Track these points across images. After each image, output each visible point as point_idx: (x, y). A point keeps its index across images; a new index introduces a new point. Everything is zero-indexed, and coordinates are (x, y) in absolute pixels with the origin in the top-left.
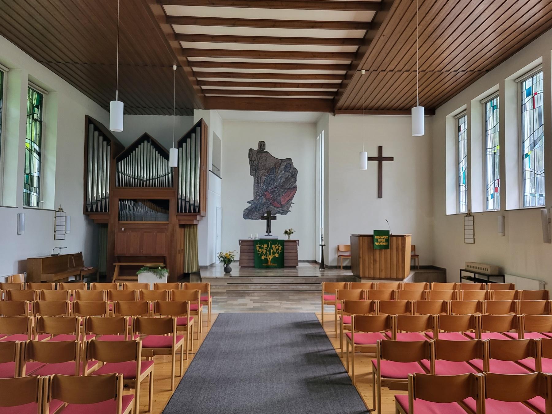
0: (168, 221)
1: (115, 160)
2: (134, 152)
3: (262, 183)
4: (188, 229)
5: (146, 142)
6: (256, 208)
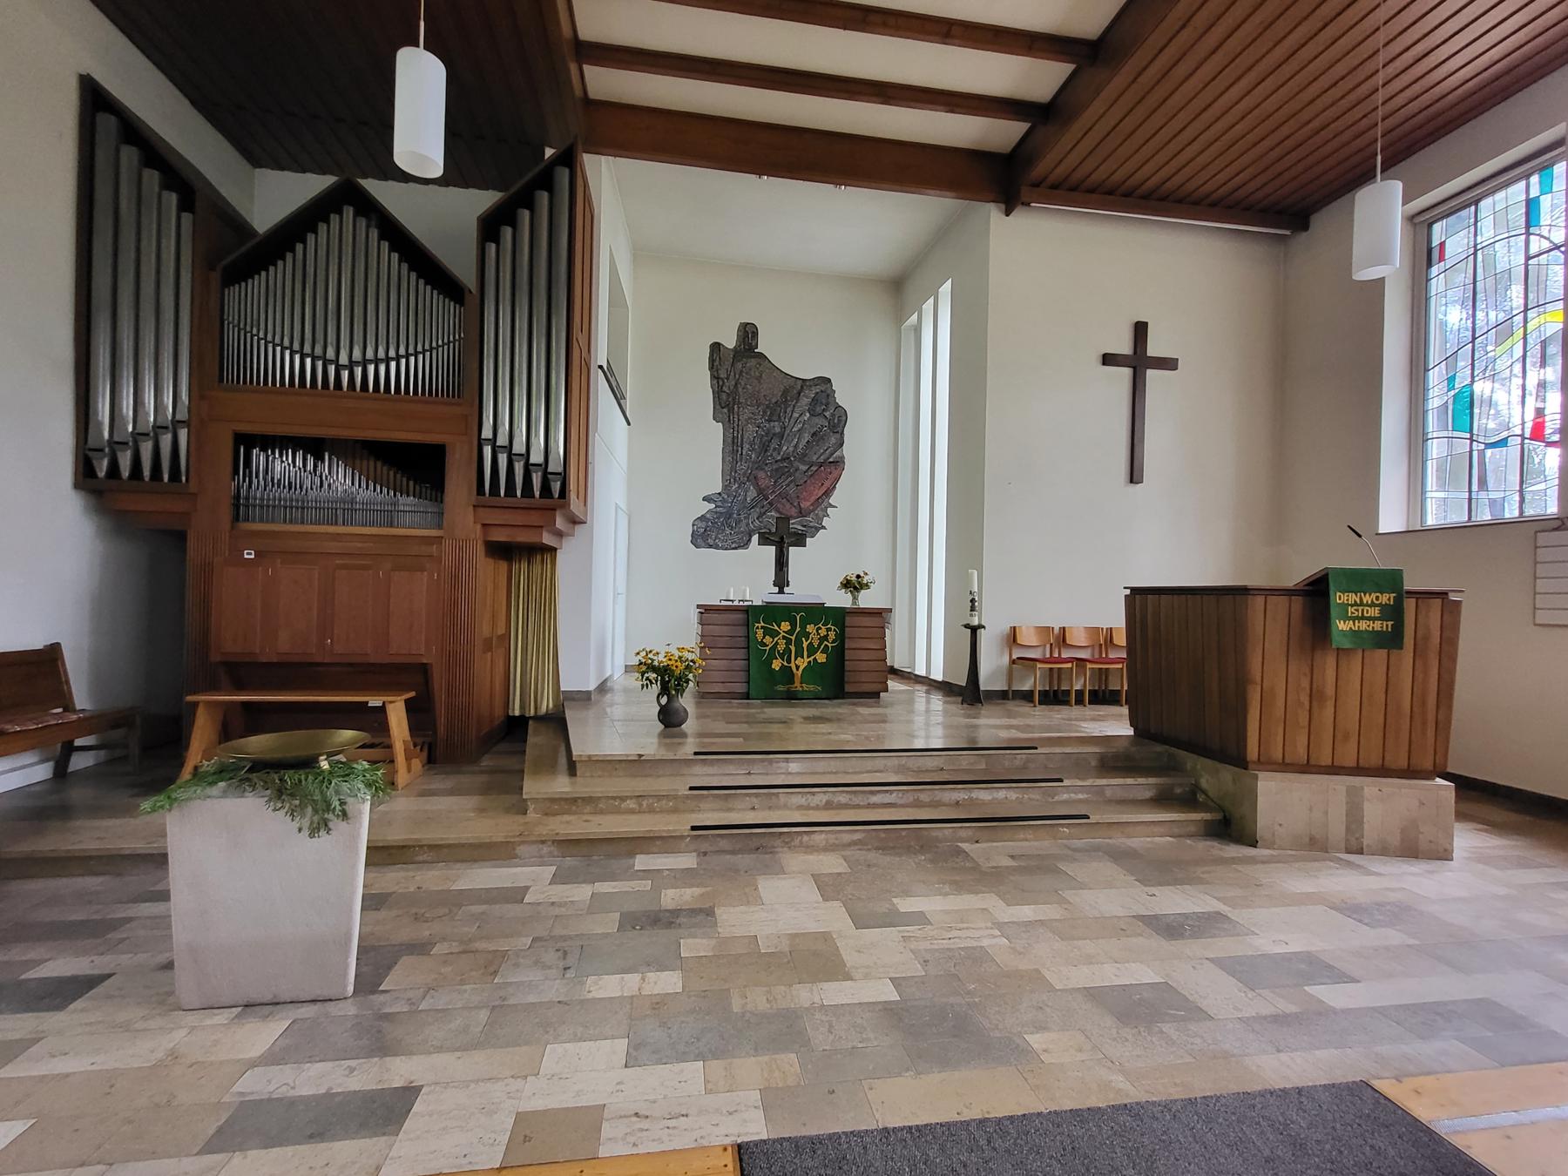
0: (440, 527)
1: (216, 277)
3: (746, 446)
4: (524, 565)
5: (349, 212)
6: (729, 515)
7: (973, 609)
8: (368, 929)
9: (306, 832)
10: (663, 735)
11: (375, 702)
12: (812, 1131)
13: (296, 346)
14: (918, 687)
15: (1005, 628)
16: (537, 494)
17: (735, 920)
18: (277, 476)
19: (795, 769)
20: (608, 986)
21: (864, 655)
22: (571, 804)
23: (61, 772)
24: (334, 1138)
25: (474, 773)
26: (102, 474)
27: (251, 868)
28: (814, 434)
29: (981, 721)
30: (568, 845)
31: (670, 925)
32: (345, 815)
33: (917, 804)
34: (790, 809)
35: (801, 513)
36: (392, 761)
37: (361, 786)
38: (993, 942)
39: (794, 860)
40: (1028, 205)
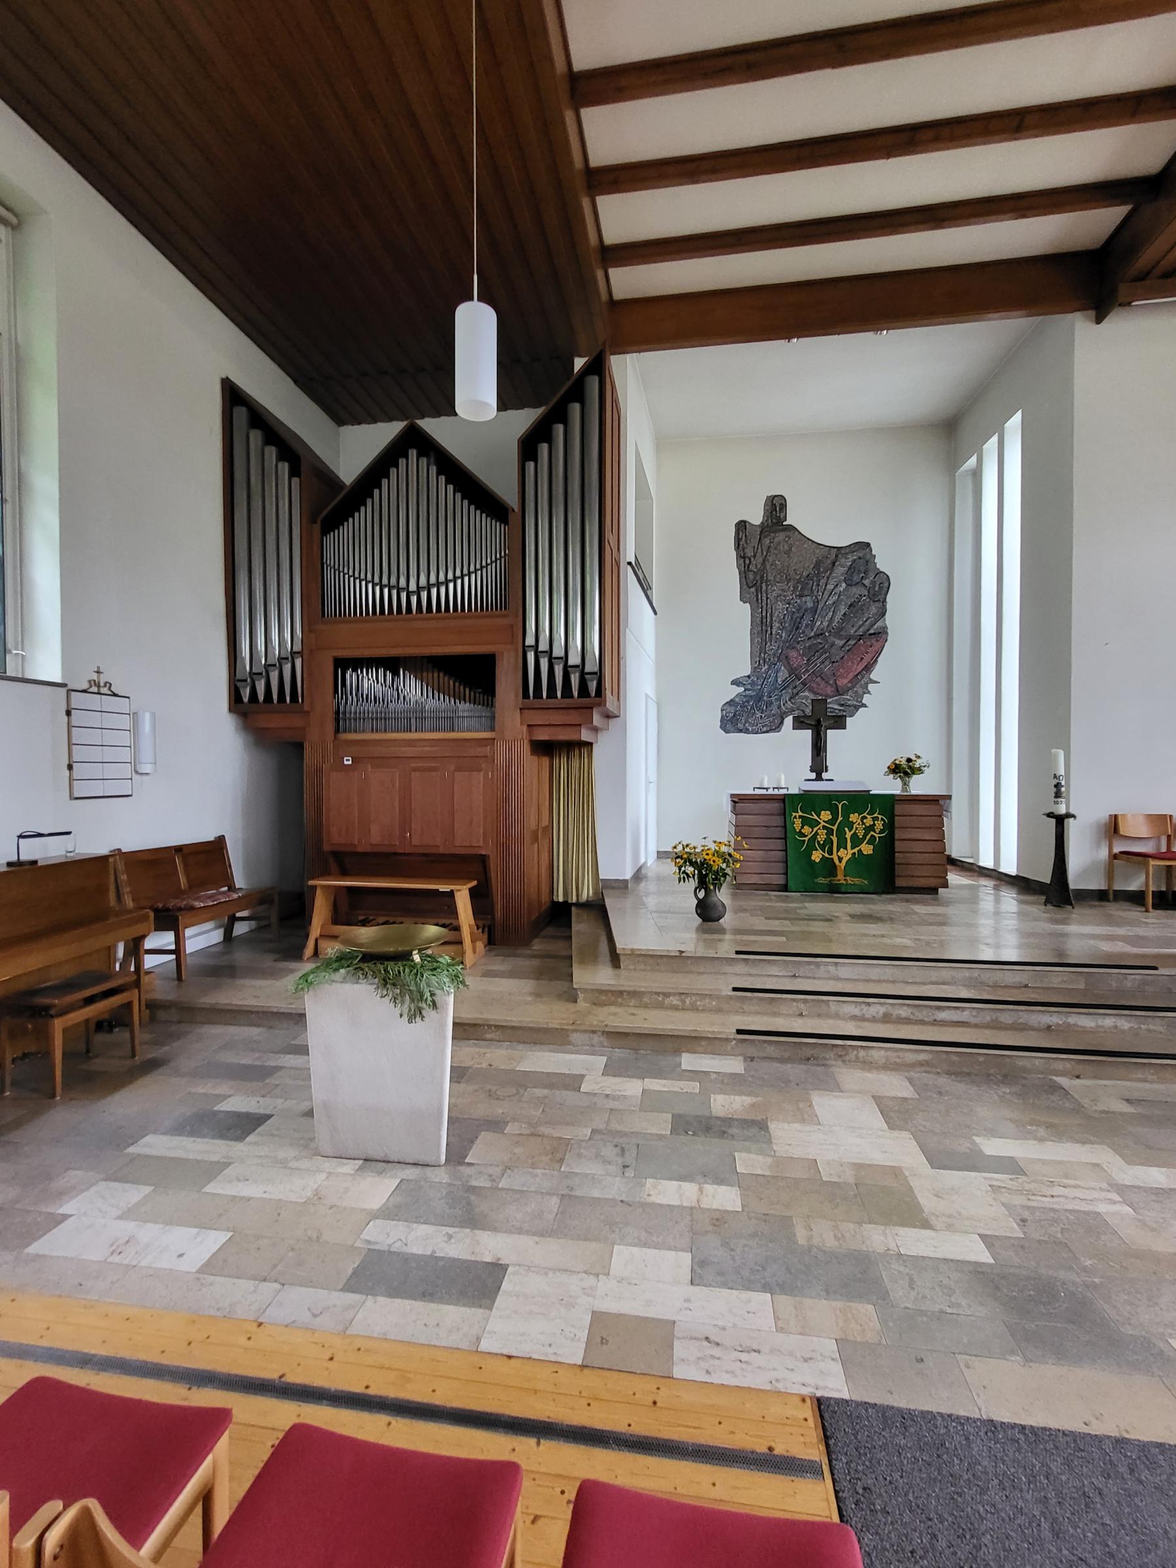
0: (492, 729)
1: (317, 528)
2: (376, 492)
4: (564, 760)
5: (413, 453)
6: (759, 698)
7: (1058, 795)
8: (453, 1101)
9: (405, 1018)
10: (700, 930)
11: (444, 888)
12: (900, 1401)
13: (377, 580)
14: (983, 881)
15: (1102, 814)
16: (576, 694)
17: (791, 1137)
18: (365, 692)
19: (848, 976)
20: (670, 1192)
22: (613, 996)
23: (228, 937)
24: (441, 1301)
25: (525, 956)
26: (246, 700)
27: (371, 1046)
29: (1073, 928)
30: (618, 1037)
31: (723, 1134)
32: (434, 1005)
33: (995, 1026)
34: (842, 1019)
35: (838, 692)
36: (461, 943)
37: (446, 980)
38: (1112, 1209)
39: (849, 1076)
40: (1129, 304)
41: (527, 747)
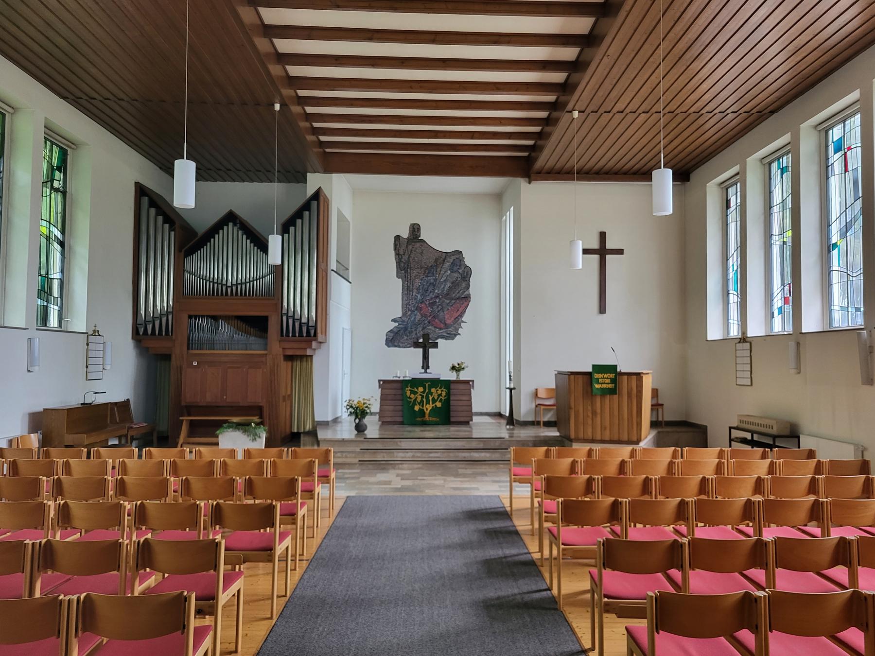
0: (266, 349)
1: (182, 253)
4: (298, 363)
5: (231, 225)
6: (406, 329)
21: (461, 403)
26: (141, 333)
28: (452, 283)
34: (400, 455)
41: (282, 358)
